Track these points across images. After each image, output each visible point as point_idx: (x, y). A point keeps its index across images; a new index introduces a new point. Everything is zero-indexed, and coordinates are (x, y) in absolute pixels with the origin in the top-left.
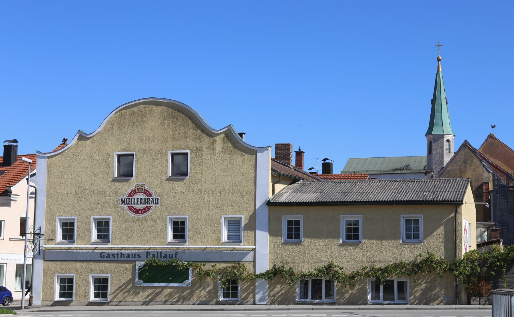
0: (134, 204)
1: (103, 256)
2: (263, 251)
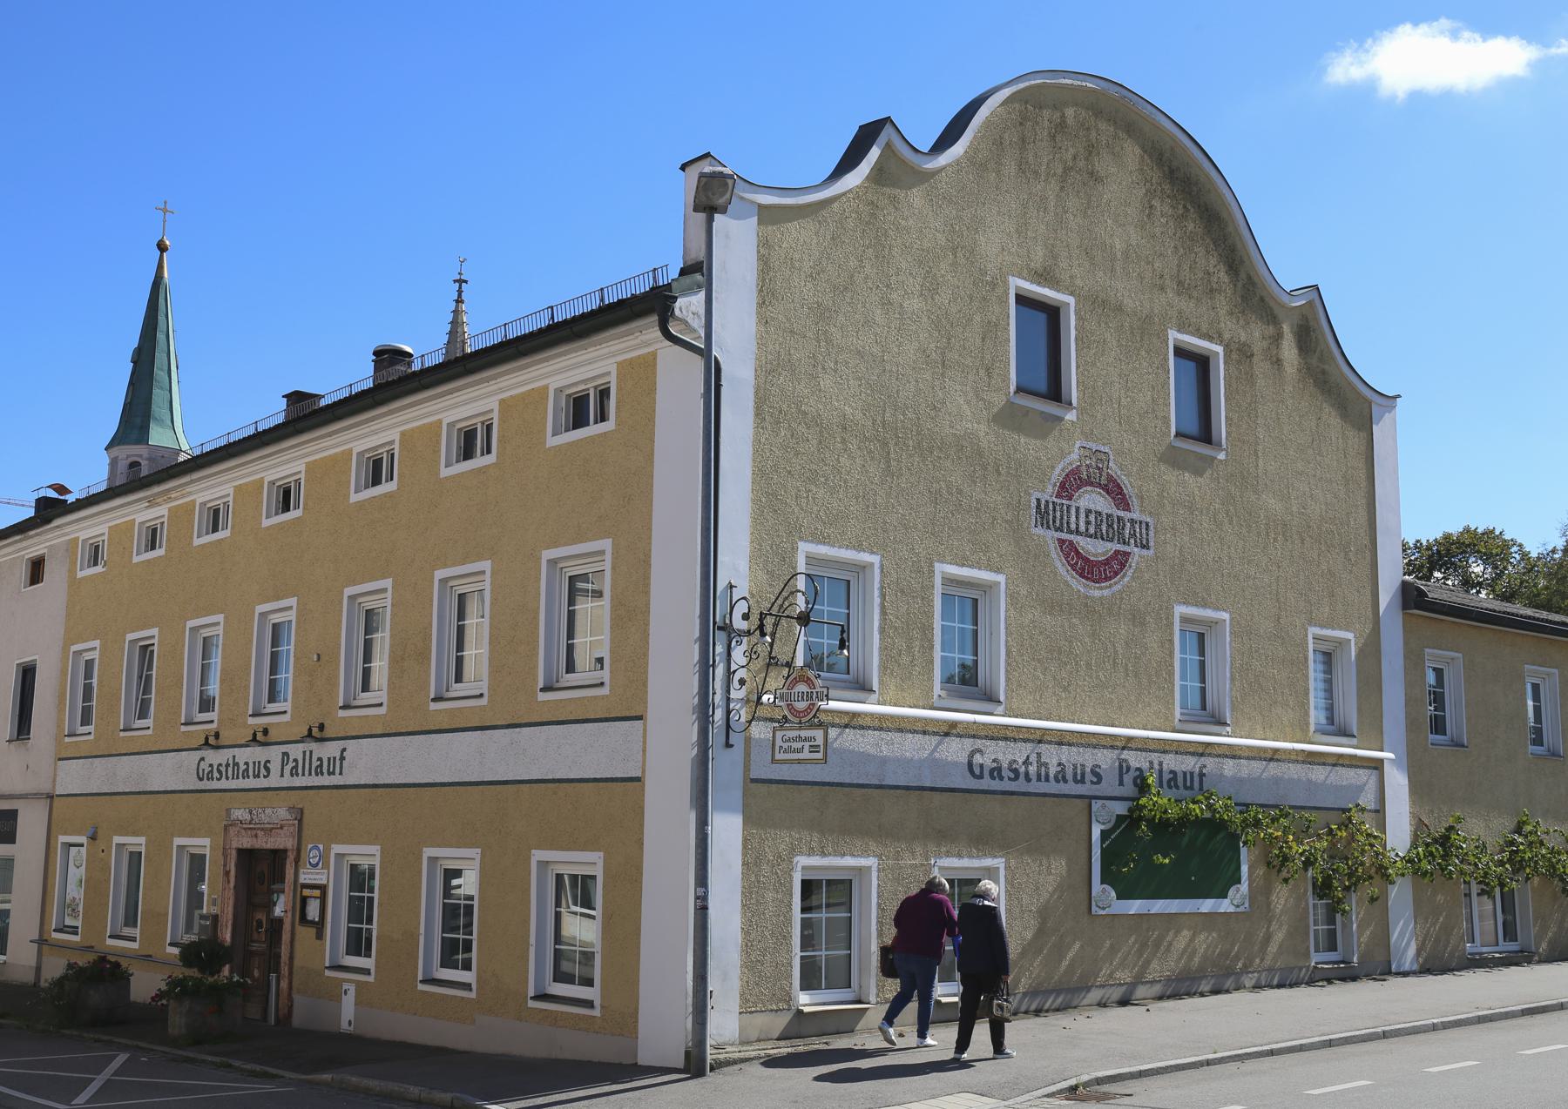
0: (1077, 532)
1: (977, 771)
2: (768, 639)
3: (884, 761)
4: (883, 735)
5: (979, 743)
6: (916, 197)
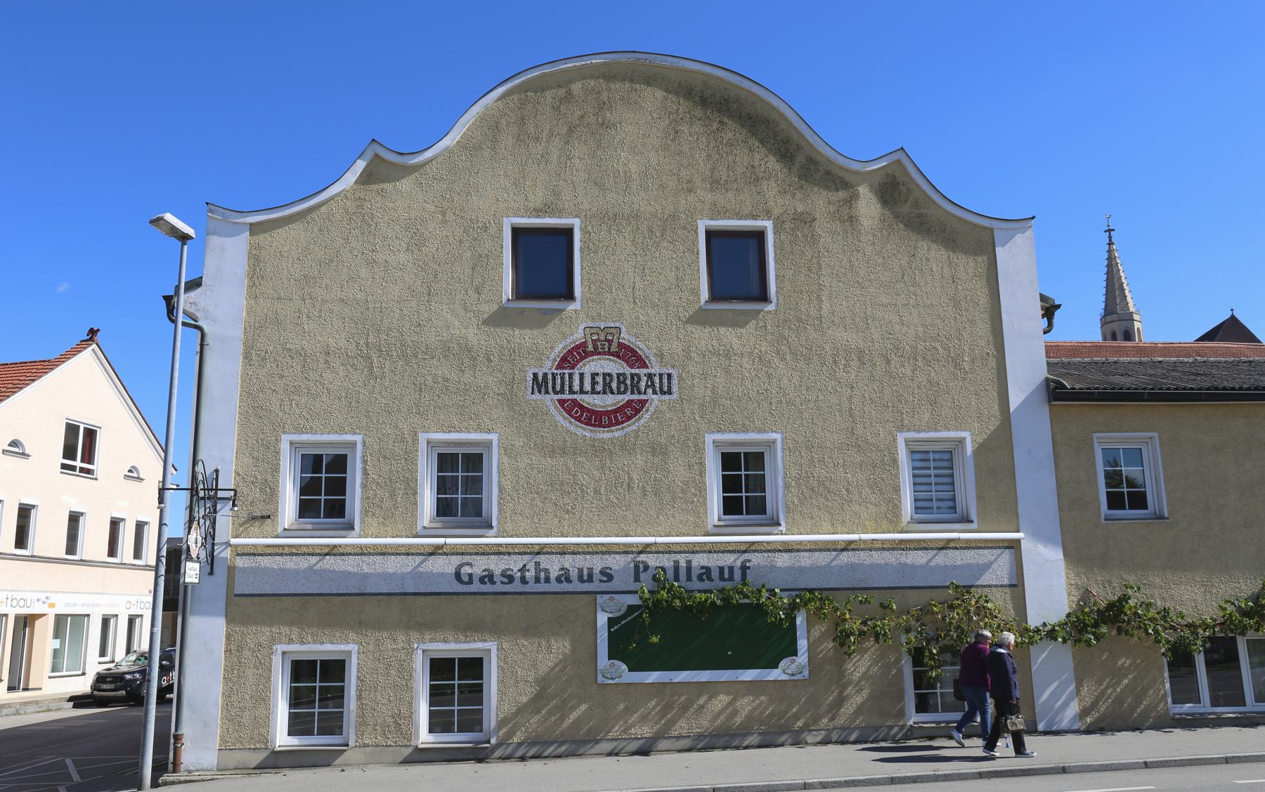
0: (582, 391)
1: (466, 579)
3: (365, 576)
4: (365, 558)
5: (467, 559)
6: (406, 184)
